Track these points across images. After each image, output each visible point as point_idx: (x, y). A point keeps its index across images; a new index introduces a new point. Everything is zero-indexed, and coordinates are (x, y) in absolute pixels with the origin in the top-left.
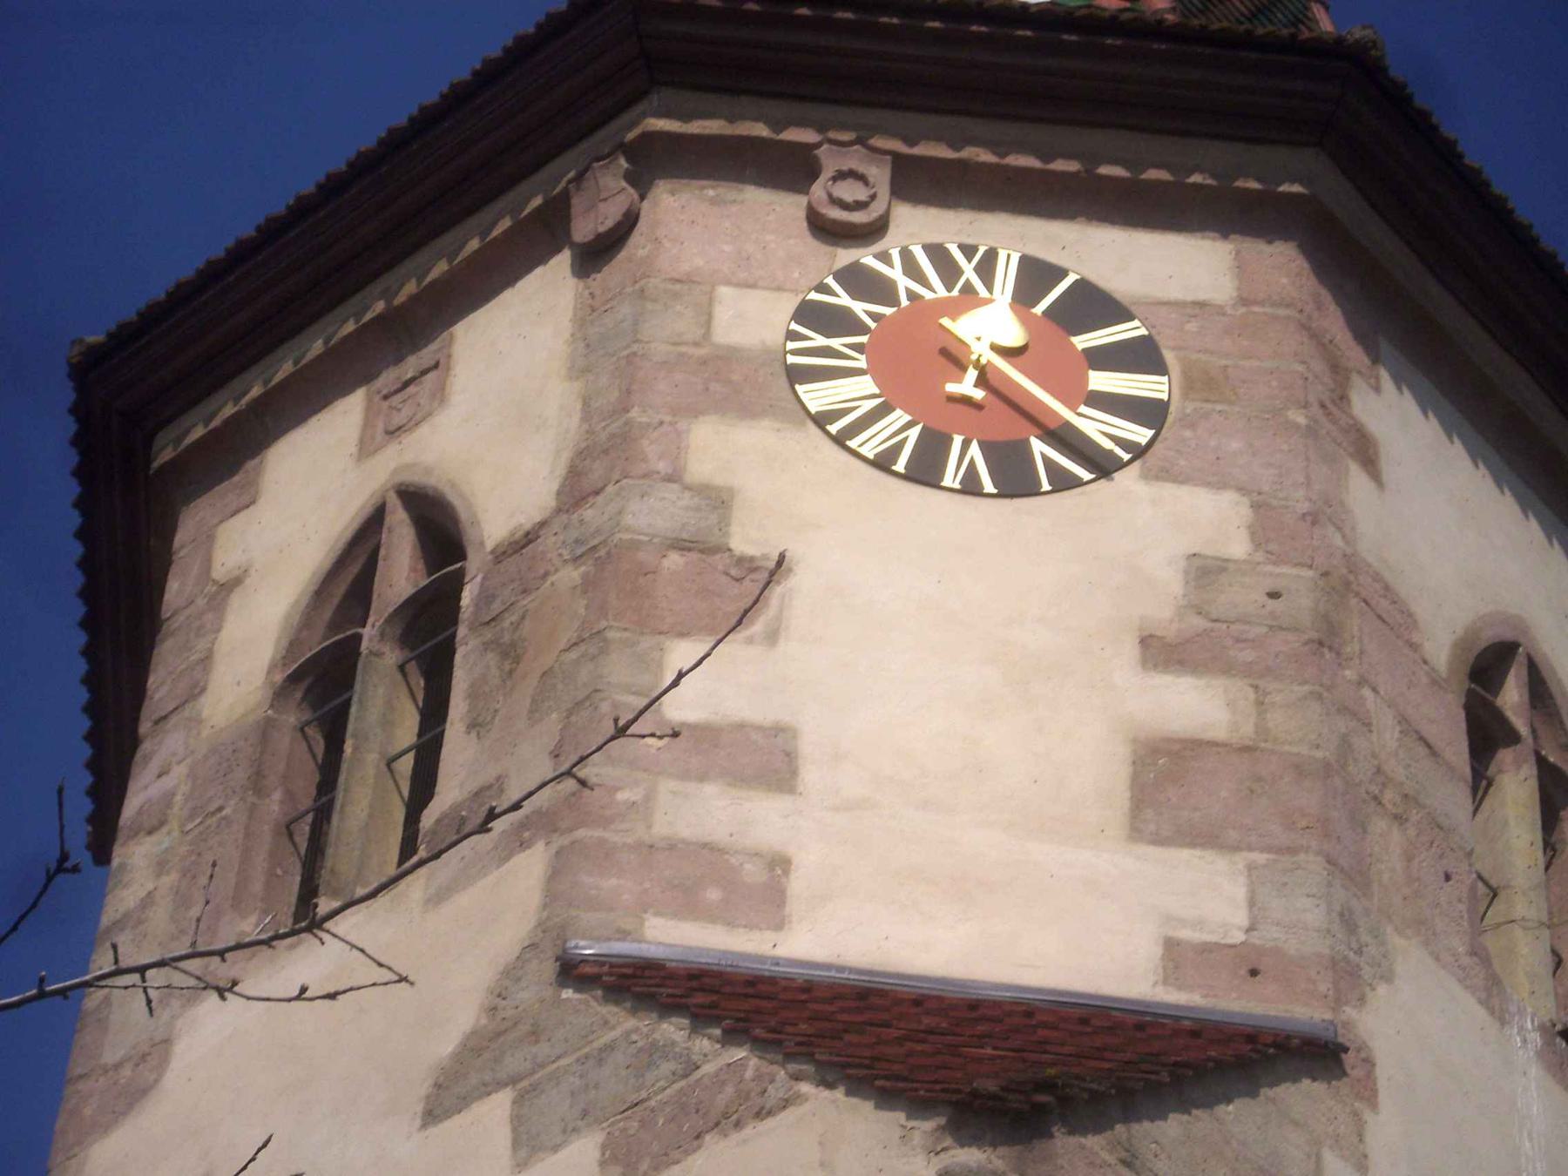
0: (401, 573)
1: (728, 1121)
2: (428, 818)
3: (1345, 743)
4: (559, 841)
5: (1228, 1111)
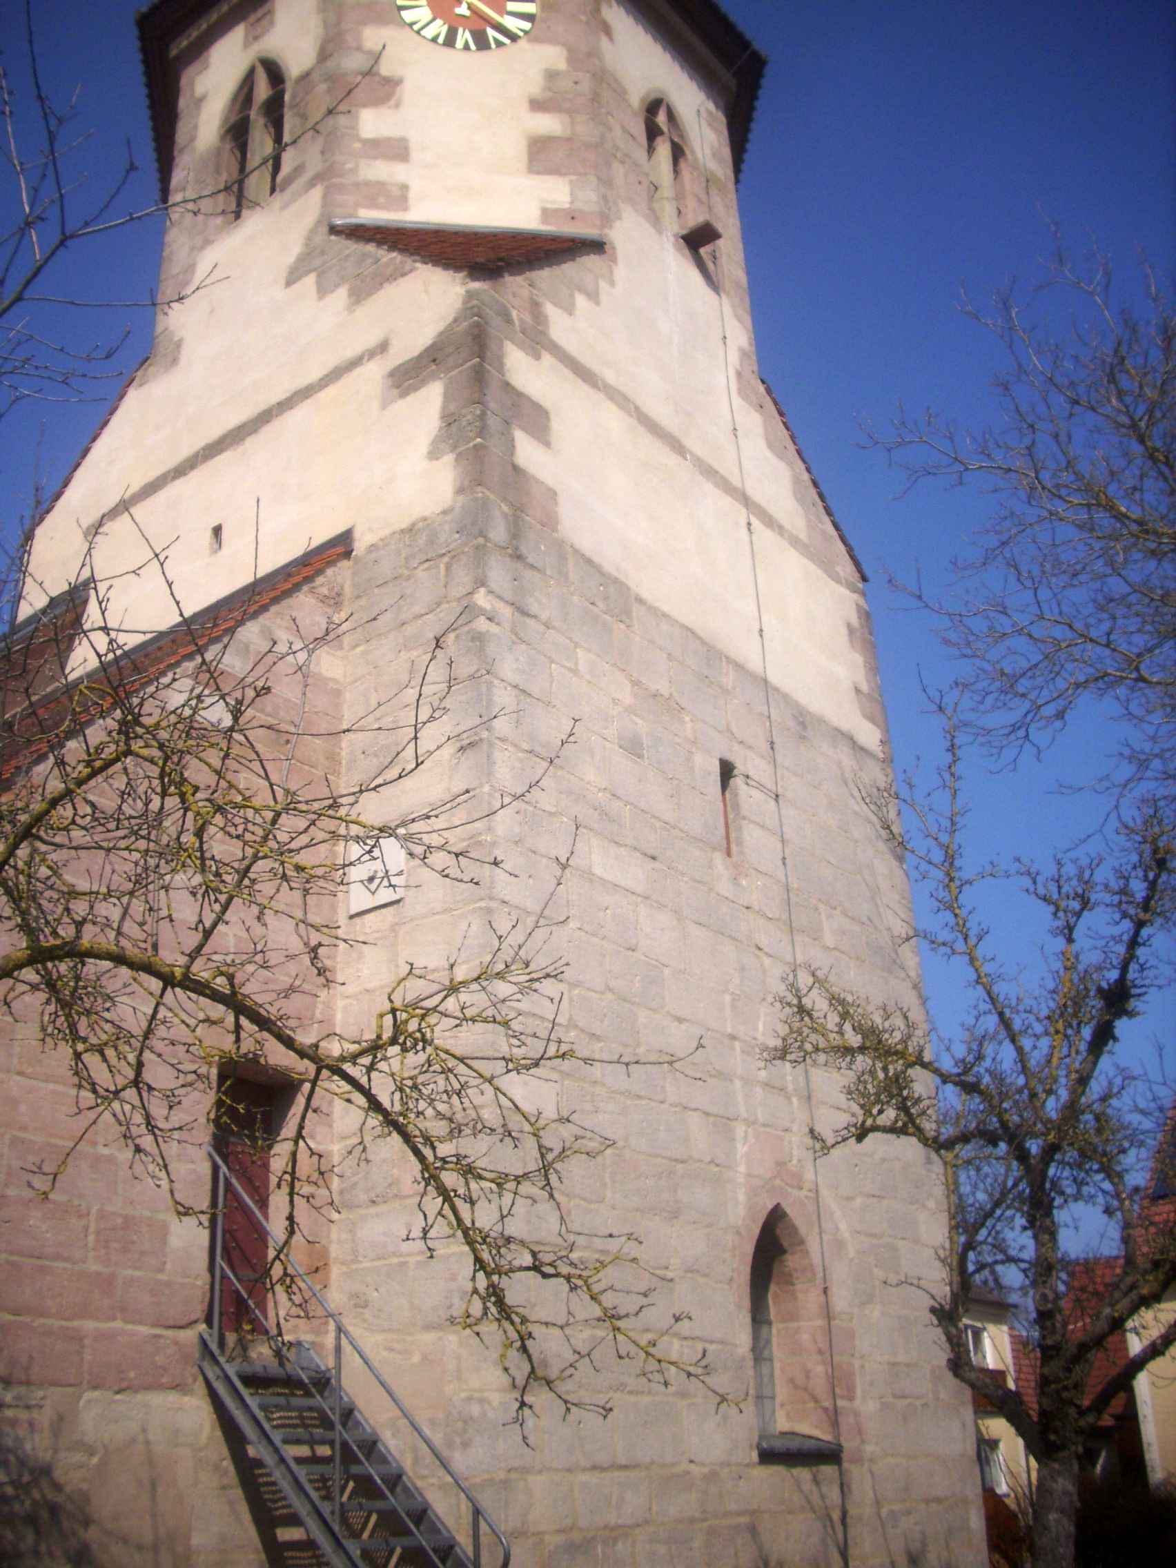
0: (263, 91)
1: (392, 278)
2: (279, 179)
3: (602, 137)
4: (326, 183)
5: (565, 266)
